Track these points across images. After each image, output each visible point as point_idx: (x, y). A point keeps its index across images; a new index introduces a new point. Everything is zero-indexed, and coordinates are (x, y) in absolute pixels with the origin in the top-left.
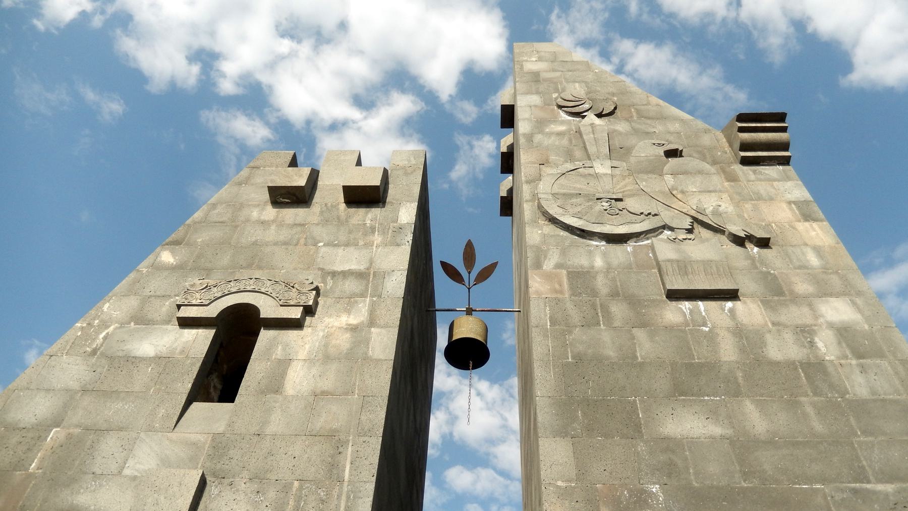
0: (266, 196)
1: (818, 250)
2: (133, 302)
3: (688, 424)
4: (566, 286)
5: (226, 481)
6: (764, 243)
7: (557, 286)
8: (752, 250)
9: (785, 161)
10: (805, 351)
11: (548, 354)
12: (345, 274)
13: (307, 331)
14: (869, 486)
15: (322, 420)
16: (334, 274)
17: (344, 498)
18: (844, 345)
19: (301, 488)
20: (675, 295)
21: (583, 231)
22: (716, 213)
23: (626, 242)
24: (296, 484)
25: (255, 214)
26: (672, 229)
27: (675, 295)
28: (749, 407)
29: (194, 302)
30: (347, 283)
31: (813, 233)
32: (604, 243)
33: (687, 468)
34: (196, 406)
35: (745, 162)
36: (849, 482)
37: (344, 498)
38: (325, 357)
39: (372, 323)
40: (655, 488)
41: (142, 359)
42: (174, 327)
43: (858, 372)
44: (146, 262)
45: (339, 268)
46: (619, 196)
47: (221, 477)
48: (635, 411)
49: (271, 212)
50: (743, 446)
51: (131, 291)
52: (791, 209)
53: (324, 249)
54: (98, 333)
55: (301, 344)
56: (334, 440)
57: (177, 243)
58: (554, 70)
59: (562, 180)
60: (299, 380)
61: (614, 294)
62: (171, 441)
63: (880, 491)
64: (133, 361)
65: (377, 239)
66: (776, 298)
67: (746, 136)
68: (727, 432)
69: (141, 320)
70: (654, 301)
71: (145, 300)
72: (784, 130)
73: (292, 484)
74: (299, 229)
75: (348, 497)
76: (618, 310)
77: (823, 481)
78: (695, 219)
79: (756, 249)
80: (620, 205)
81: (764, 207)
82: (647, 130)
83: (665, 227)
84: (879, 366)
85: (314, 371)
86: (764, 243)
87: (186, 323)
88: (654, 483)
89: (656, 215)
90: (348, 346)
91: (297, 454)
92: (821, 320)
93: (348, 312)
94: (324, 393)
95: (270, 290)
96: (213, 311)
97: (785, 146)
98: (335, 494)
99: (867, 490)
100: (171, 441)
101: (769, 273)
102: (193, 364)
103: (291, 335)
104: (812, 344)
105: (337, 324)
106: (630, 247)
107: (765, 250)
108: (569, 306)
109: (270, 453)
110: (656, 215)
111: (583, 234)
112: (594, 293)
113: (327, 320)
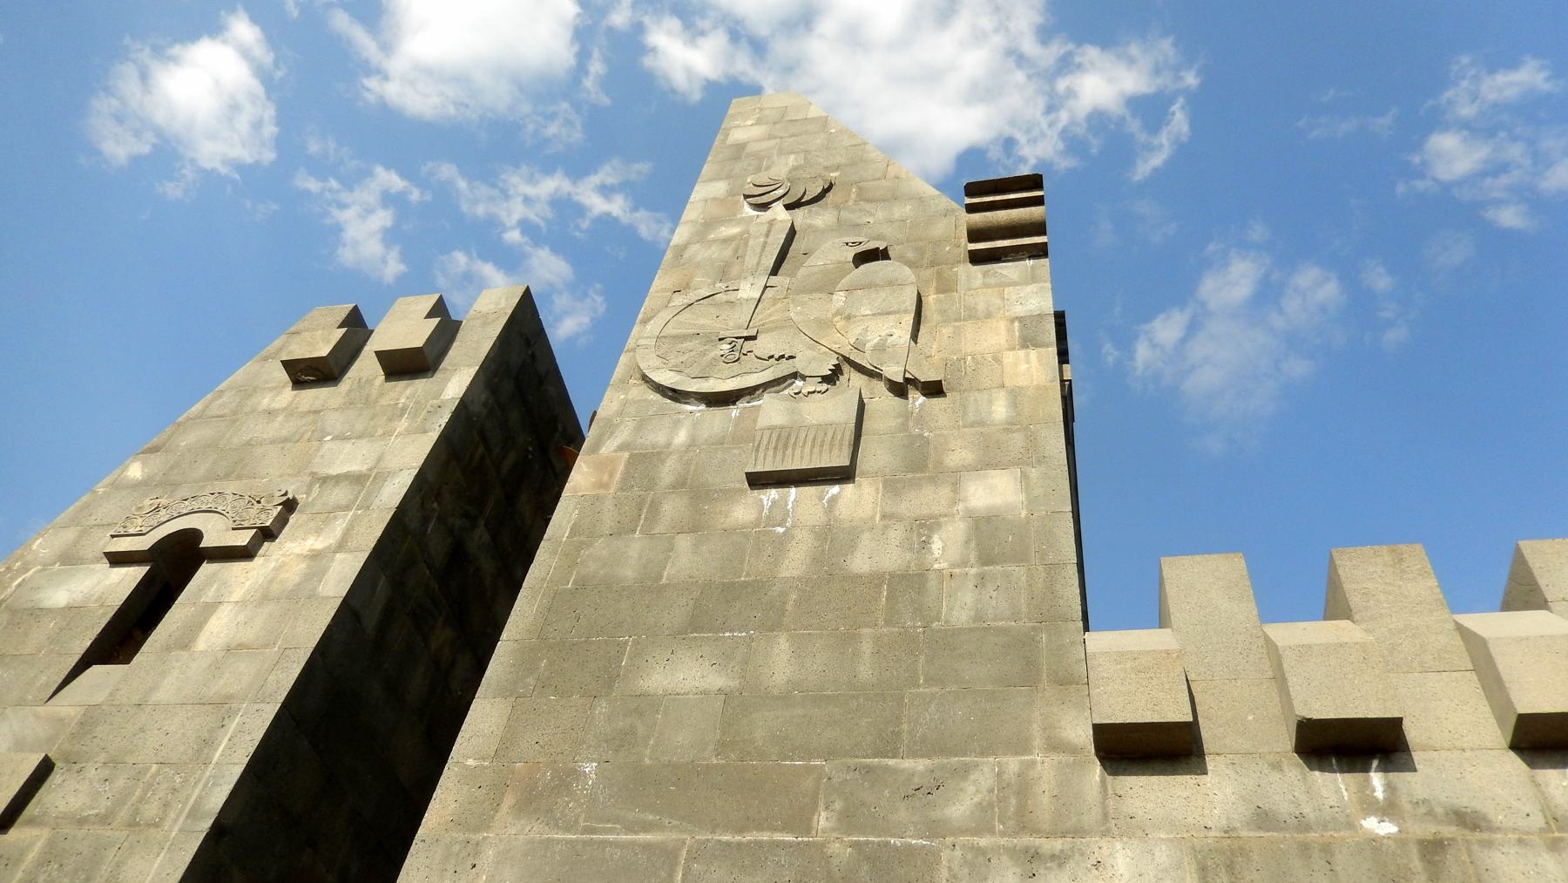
0: (283, 375)
1: (1015, 396)
2: (69, 535)
3: (686, 675)
4: (618, 476)
5: (77, 767)
6: (934, 389)
7: (606, 478)
8: (915, 400)
9: (1040, 252)
10: (909, 555)
11: (543, 580)
12: (338, 479)
13: (258, 561)
14: (891, 762)
15: (221, 682)
16: (325, 480)
17: (201, 785)
18: (973, 545)
19: (158, 773)
20: (758, 481)
21: (674, 391)
22: (880, 348)
23: (734, 403)
24: (154, 768)
25: (266, 401)
26: (804, 378)
27: (758, 481)
28: (783, 644)
29: (131, 531)
30: (336, 491)
31: (1024, 367)
32: (703, 407)
33: (648, 738)
34: (96, 670)
35: (977, 258)
36: (867, 756)
37: (201, 785)
38: (264, 597)
39: (341, 546)
40: (589, 768)
41: (50, 610)
42: (105, 564)
43: (971, 586)
44: (108, 480)
45: (333, 472)
46: (752, 332)
47: (71, 760)
48: (621, 653)
49: (288, 394)
50: (737, 705)
51: (74, 521)
52: (1010, 331)
53: (332, 445)
54: (13, 579)
55: (240, 578)
56: (222, 706)
57: (155, 450)
58: (770, 137)
59: (686, 315)
60: (218, 630)
61: (679, 485)
62: (36, 716)
63: (903, 770)
64: (38, 613)
65: (403, 424)
66: (910, 475)
67: (979, 218)
68: (731, 684)
69: (70, 559)
70: (730, 490)
71: (85, 532)
72: (1039, 201)
73: (148, 769)
74: (312, 417)
75: (205, 785)
76: (673, 508)
77: (830, 753)
78: (847, 360)
79: (922, 399)
80: (748, 345)
81: (969, 328)
82: (859, 221)
83: (795, 375)
84: (1007, 575)
85: (241, 618)
86: (934, 389)
87: (117, 559)
88: (593, 760)
89: (791, 357)
90: (297, 579)
91: (172, 729)
92: (961, 506)
93: (318, 531)
94: (240, 646)
95: (213, 506)
96: (143, 544)
97: (1039, 228)
98: (192, 781)
99: (887, 768)
100: (36, 716)
101: (921, 436)
102: (104, 615)
103: (238, 567)
104: (925, 545)
105: (298, 550)
106: (734, 411)
107: (935, 401)
108: (608, 505)
109: (142, 730)
110: (791, 357)
111: (676, 395)
112: (651, 484)
113: (288, 545)
